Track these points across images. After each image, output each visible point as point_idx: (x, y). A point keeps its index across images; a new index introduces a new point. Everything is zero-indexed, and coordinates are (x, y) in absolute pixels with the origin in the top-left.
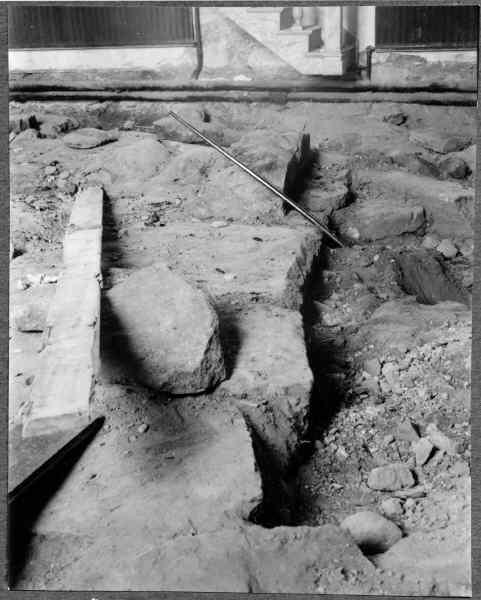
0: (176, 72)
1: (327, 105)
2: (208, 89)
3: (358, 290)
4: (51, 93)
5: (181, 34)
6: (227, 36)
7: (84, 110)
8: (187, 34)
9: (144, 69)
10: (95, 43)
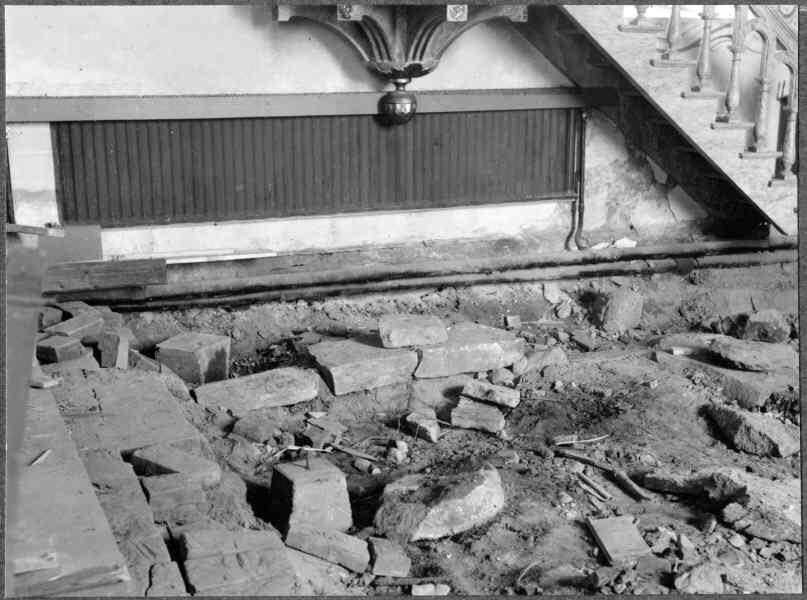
0: (541, 238)
1: (736, 270)
2: (611, 261)
3: (381, 468)
4: (389, 283)
5: (560, 186)
6: (609, 185)
7: (517, 317)
8: (428, 193)
9: (500, 236)
10: (444, 201)
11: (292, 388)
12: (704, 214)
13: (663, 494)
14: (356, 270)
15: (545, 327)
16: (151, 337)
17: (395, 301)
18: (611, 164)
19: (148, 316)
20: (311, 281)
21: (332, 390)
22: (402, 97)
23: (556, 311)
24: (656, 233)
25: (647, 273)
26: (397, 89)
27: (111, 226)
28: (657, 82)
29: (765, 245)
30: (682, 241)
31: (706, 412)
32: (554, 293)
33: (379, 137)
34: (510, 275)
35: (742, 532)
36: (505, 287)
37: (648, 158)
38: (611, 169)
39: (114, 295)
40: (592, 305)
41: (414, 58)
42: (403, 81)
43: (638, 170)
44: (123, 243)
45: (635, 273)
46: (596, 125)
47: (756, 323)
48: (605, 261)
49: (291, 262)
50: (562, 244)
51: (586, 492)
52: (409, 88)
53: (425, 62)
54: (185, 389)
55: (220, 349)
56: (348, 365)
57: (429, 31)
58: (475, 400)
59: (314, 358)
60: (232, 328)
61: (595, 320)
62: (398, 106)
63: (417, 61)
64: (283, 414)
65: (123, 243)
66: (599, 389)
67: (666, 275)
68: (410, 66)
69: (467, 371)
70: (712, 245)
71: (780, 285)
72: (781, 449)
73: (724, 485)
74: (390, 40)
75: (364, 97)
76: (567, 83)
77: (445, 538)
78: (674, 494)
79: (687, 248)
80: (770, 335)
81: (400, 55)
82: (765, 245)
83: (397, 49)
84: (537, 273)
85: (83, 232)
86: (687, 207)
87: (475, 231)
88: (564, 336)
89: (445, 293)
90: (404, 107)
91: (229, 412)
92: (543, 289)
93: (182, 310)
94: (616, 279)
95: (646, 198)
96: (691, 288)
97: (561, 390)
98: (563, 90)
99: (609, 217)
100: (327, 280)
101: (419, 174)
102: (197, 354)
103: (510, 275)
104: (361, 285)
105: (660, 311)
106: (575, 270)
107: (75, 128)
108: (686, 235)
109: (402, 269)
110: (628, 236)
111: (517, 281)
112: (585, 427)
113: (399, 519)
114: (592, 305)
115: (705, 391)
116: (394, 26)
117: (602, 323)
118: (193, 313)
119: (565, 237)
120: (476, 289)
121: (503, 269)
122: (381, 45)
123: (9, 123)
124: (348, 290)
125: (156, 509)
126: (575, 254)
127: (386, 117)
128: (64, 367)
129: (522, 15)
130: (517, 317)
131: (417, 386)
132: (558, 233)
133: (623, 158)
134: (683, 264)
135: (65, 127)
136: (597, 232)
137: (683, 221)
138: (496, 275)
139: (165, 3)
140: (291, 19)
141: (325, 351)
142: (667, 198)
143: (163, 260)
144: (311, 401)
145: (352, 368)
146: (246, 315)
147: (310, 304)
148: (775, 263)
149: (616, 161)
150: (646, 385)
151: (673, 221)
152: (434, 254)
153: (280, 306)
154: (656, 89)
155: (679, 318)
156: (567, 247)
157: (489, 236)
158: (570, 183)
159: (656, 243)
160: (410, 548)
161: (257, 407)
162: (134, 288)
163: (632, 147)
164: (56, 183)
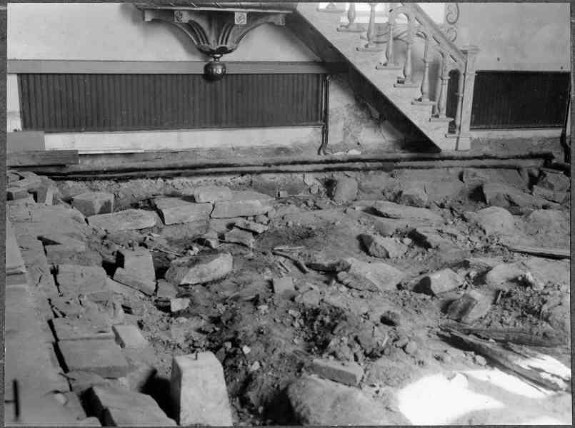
2: (343, 162)
4: (210, 170)
6: (345, 118)
9: (279, 146)
11: (141, 220)
12: (401, 136)
13: (318, 271)
14: (190, 161)
15: (302, 198)
16: (71, 194)
17: (215, 181)
18: (345, 106)
19: (70, 183)
20: (163, 166)
21: (164, 223)
22: (216, 65)
23: (310, 190)
24: (374, 148)
25: (366, 170)
26: (215, 60)
27: (51, 132)
28: (361, 60)
29: (437, 156)
30: (389, 152)
31: (360, 238)
32: (310, 180)
33: (205, 87)
34: (282, 168)
35: (347, 286)
36: (282, 175)
37: (368, 104)
38: (345, 109)
39: (52, 170)
40: (330, 185)
41: (222, 43)
42: (218, 56)
43: (363, 110)
44: (57, 142)
45: (358, 170)
46: (336, 83)
47: (406, 196)
48: (339, 162)
49: (154, 157)
50: (317, 152)
51: (279, 269)
52: (221, 59)
53: (228, 46)
54: (82, 217)
55: (107, 201)
56: (172, 209)
57: (228, 31)
58: (241, 229)
59: (156, 205)
60: (118, 192)
61: (330, 195)
62: (215, 70)
63: (224, 45)
64: (137, 234)
65: (57, 142)
66: (310, 226)
67: (378, 172)
68: (223, 47)
69: (241, 215)
70: (404, 155)
71: (443, 180)
72: (390, 255)
73: (343, 265)
74: (208, 33)
75: (196, 65)
76: (319, 59)
77: (198, 284)
78: (324, 271)
79: (390, 156)
80: (415, 202)
81: (214, 41)
82: (437, 156)
83: (212, 39)
84: (298, 167)
85: (33, 134)
86: (392, 133)
87: (264, 143)
88: (311, 203)
89: (245, 177)
90: (219, 70)
91: (106, 231)
92: (304, 177)
93: (90, 180)
94: (346, 172)
95: (367, 127)
96: (391, 179)
97: (291, 226)
98: (315, 63)
99: (344, 137)
100: (172, 166)
101: (229, 107)
102: (94, 202)
103: (282, 168)
104: (194, 170)
105: (372, 192)
106: (321, 167)
107: (31, 78)
108: (391, 149)
109: (218, 162)
110: (356, 148)
111: (287, 172)
112: (294, 243)
113: (176, 274)
114: (330, 185)
115: (364, 227)
116: (210, 26)
117: (333, 197)
118: (96, 183)
119: (318, 148)
120: (264, 176)
121: (278, 164)
122: (203, 35)
123: (10, 74)
124: (186, 173)
125: (50, 259)
126: (322, 157)
127: (209, 76)
128: (17, 202)
129: (281, 21)
130: (286, 192)
131: (212, 222)
132: (314, 145)
133: (351, 102)
134: (387, 165)
135: (25, 76)
136: (337, 146)
137: (389, 141)
138: (274, 168)
139: (4, 38)
140: (153, 20)
141: (161, 203)
142: (379, 127)
143: (77, 151)
144: (152, 228)
145: (175, 212)
146: (127, 185)
147: (164, 181)
148: (444, 167)
149: (349, 105)
150: (334, 224)
151: (384, 141)
152: (239, 155)
153: (147, 181)
154: (361, 64)
155: (382, 196)
156: (319, 153)
157: (272, 145)
158: (320, 117)
159: (373, 153)
160: (180, 288)
161: (122, 229)
162: (62, 166)
163: (358, 97)
164: (20, 108)
